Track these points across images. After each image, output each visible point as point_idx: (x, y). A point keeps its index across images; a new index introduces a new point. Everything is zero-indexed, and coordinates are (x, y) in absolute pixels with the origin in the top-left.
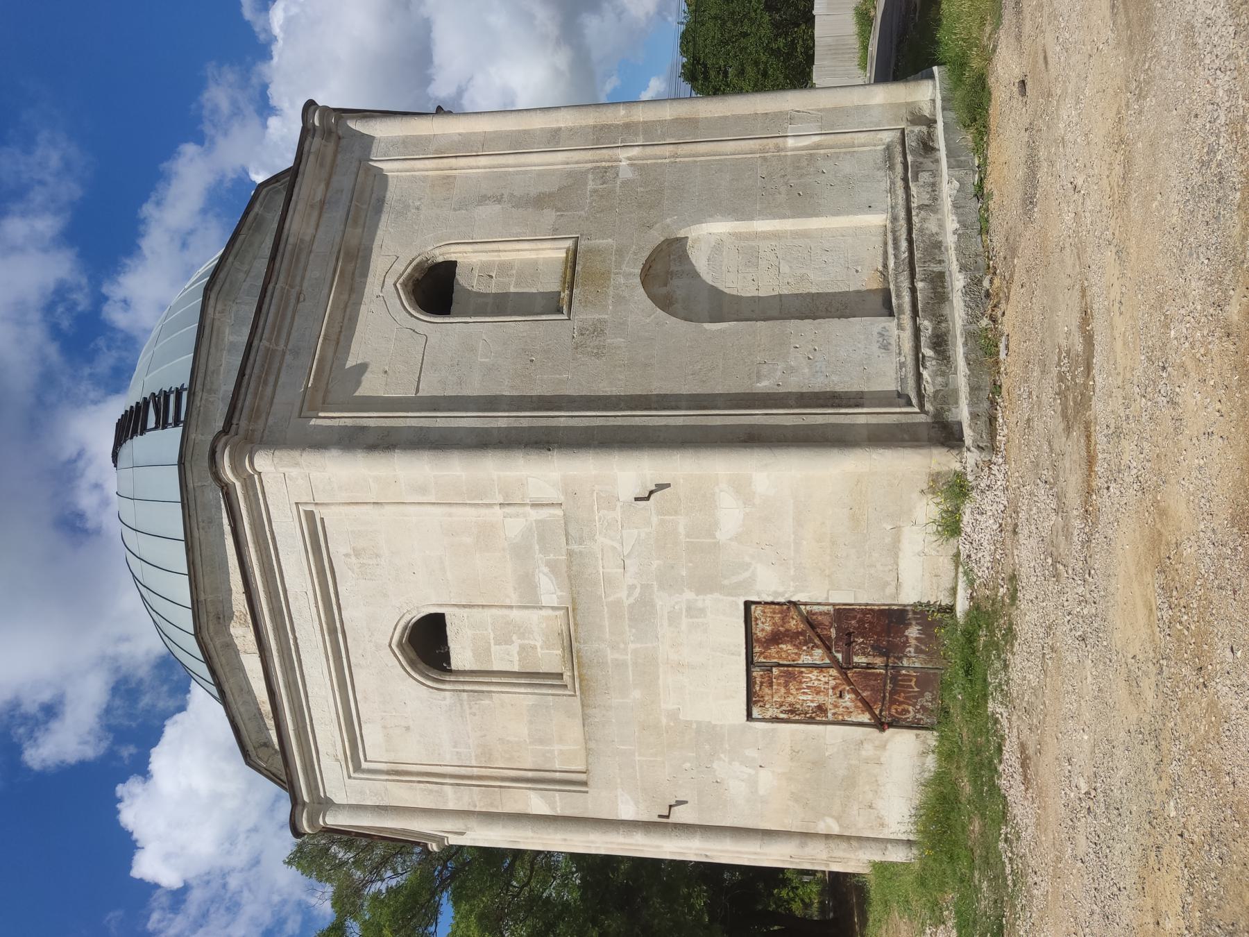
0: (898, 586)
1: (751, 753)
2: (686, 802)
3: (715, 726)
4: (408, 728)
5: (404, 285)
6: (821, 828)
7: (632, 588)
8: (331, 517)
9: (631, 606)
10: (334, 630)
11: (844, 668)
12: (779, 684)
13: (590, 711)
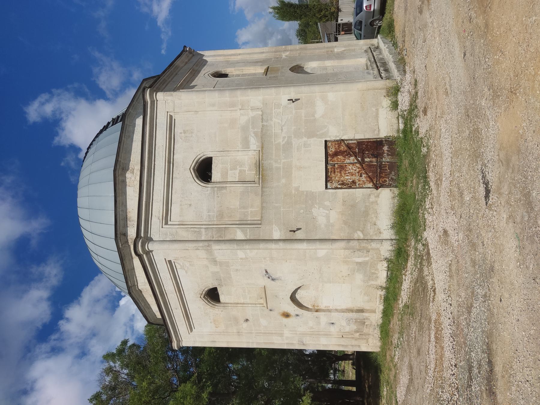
0: (379, 131)
1: (327, 203)
2: (300, 229)
3: (313, 192)
4: (190, 205)
5: (194, 169)
6: (356, 236)
7: (284, 138)
8: (177, 118)
9: (284, 145)
10: (170, 162)
11: (362, 163)
12: (338, 172)
13: (265, 190)
